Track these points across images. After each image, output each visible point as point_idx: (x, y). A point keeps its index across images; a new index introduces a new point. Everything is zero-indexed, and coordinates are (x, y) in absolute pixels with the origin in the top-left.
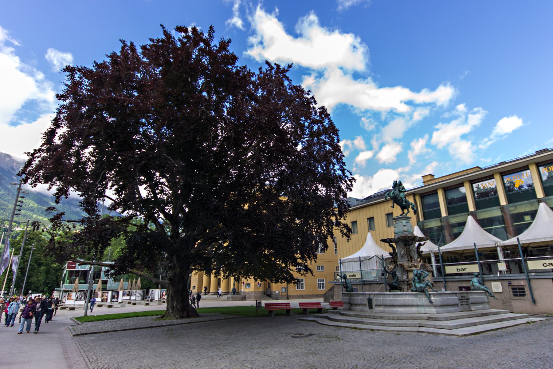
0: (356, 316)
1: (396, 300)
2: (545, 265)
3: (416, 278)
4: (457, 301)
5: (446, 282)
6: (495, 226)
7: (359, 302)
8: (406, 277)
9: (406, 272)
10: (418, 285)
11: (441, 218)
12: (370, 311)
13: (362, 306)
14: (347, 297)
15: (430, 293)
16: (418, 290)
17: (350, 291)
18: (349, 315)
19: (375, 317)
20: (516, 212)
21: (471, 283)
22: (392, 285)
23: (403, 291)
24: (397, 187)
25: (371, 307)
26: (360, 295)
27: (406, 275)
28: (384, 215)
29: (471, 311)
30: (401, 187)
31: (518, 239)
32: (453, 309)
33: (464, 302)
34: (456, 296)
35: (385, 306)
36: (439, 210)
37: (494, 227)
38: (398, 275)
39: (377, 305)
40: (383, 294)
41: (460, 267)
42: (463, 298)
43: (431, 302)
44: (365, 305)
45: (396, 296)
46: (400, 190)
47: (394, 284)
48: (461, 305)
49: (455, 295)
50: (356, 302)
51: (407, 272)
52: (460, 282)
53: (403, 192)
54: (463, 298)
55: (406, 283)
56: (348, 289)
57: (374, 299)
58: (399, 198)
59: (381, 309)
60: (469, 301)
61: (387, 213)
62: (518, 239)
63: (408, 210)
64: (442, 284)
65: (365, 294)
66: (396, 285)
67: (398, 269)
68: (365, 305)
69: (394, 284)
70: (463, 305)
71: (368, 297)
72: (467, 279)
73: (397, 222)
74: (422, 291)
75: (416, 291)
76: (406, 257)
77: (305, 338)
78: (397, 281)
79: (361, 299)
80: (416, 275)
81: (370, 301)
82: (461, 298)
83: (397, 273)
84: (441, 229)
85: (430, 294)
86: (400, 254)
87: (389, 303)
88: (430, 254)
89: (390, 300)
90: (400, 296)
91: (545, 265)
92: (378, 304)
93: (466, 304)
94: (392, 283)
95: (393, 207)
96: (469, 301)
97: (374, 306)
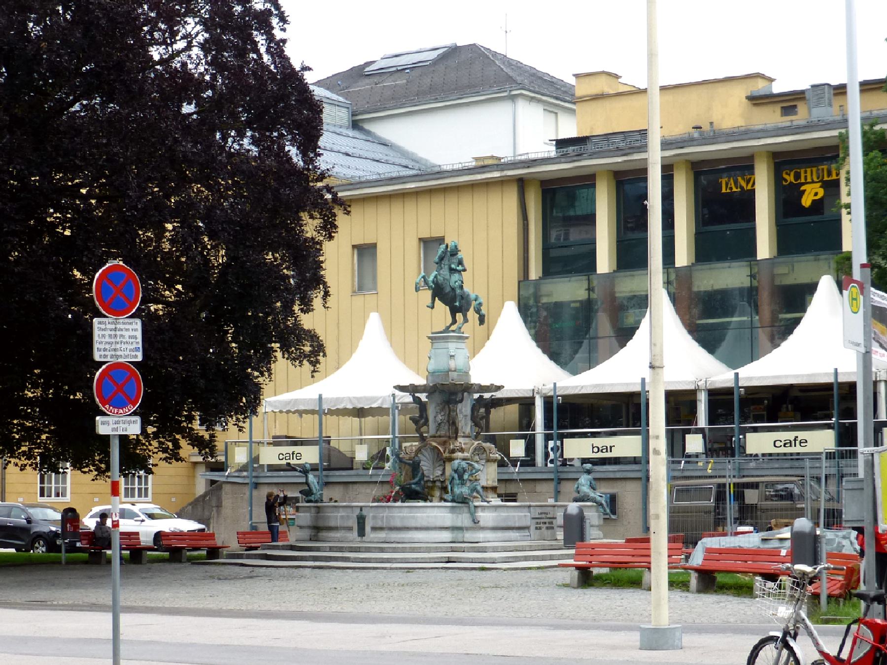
0: (331, 549)
1: (413, 517)
2: (778, 444)
3: (456, 476)
4: (527, 522)
5: (560, 480)
6: (740, 316)
7: (339, 523)
8: (440, 473)
9: (442, 462)
10: (457, 490)
11: (593, 277)
12: (359, 539)
13: (343, 531)
14: (308, 514)
15: (476, 504)
16: (456, 498)
17: (316, 502)
18: (318, 549)
19: (368, 550)
20: (790, 281)
21: (576, 486)
22: (410, 488)
23: (431, 501)
24: (446, 262)
25: (362, 532)
26: (341, 510)
27: (441, 468)
28: (415, 242)
29: (556, 540)
30: (455, 260)
31: (737, 375)
32: (517, 534)
33: (545, 523)
34: (530, 512)
35: (392, 529)
36: (592, 243)
37: (734, 319)
38: (424, 468)
39: (374, 529)
40: (388, 507)
41: (600, 442)
42: (543, 516)
43: (475, 521)
44: (350, 529)
45: (415, 510)
46: (453, 266)
47: (413, 486)
48: (536, 528)
49: (527, 509)
50: (332, 524)
51: (444, 462)
52: (295, 485)
53: (459, 272)
54: (543, 516)
55: (438, 484)
56: (312, 498)
57: (369, 516)
58: (448, 290)
59: (382, 535)
60: (554, 521)
61: (426, 235)
62: (737, 375)
63: (465, 316)
64: (550, 487)
65: (352, 507)
66: (418, 488)
67: (426, 453)
68: (350, 529)
69: (413, 486)
70: (540, 528)
71: (357, 511)
72: (612, 476)
73: (436, 345)
74: (463, 501)
75: (453, 501)
76: (446, 427)
77: (241, 581)
78: (420, 480)
79: (342, 517)
80: (456, 471)
81: (361, 520)
82: (537, 516)
83: (422, 463)
84: (587, 309)
85: (476, 507)
86: (435, 421)
87: (398, 524)
88: (533, 398)
89: (403, 518)
90: (421, 510)
91: (778, 444)
92: (377, 526)
93: (547, 528)
94: (410, 484)
95: (433, 307)
96: (554, 521)
97: (368, 528)
